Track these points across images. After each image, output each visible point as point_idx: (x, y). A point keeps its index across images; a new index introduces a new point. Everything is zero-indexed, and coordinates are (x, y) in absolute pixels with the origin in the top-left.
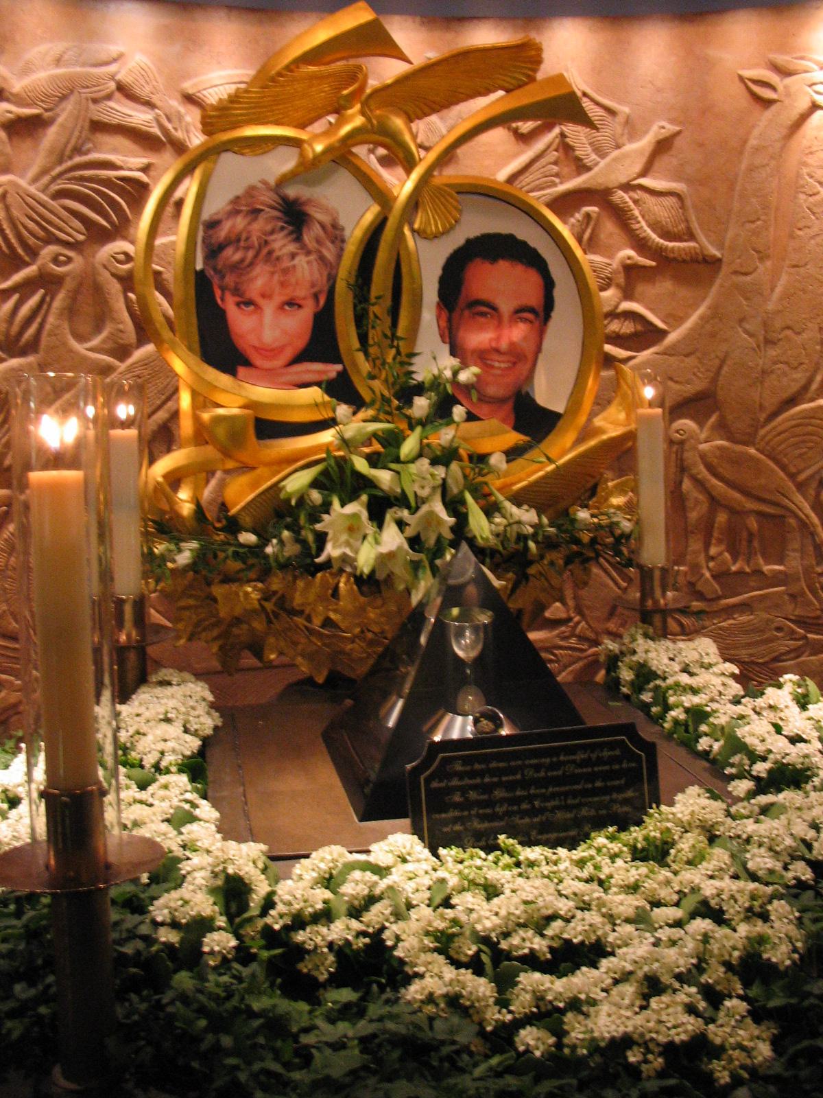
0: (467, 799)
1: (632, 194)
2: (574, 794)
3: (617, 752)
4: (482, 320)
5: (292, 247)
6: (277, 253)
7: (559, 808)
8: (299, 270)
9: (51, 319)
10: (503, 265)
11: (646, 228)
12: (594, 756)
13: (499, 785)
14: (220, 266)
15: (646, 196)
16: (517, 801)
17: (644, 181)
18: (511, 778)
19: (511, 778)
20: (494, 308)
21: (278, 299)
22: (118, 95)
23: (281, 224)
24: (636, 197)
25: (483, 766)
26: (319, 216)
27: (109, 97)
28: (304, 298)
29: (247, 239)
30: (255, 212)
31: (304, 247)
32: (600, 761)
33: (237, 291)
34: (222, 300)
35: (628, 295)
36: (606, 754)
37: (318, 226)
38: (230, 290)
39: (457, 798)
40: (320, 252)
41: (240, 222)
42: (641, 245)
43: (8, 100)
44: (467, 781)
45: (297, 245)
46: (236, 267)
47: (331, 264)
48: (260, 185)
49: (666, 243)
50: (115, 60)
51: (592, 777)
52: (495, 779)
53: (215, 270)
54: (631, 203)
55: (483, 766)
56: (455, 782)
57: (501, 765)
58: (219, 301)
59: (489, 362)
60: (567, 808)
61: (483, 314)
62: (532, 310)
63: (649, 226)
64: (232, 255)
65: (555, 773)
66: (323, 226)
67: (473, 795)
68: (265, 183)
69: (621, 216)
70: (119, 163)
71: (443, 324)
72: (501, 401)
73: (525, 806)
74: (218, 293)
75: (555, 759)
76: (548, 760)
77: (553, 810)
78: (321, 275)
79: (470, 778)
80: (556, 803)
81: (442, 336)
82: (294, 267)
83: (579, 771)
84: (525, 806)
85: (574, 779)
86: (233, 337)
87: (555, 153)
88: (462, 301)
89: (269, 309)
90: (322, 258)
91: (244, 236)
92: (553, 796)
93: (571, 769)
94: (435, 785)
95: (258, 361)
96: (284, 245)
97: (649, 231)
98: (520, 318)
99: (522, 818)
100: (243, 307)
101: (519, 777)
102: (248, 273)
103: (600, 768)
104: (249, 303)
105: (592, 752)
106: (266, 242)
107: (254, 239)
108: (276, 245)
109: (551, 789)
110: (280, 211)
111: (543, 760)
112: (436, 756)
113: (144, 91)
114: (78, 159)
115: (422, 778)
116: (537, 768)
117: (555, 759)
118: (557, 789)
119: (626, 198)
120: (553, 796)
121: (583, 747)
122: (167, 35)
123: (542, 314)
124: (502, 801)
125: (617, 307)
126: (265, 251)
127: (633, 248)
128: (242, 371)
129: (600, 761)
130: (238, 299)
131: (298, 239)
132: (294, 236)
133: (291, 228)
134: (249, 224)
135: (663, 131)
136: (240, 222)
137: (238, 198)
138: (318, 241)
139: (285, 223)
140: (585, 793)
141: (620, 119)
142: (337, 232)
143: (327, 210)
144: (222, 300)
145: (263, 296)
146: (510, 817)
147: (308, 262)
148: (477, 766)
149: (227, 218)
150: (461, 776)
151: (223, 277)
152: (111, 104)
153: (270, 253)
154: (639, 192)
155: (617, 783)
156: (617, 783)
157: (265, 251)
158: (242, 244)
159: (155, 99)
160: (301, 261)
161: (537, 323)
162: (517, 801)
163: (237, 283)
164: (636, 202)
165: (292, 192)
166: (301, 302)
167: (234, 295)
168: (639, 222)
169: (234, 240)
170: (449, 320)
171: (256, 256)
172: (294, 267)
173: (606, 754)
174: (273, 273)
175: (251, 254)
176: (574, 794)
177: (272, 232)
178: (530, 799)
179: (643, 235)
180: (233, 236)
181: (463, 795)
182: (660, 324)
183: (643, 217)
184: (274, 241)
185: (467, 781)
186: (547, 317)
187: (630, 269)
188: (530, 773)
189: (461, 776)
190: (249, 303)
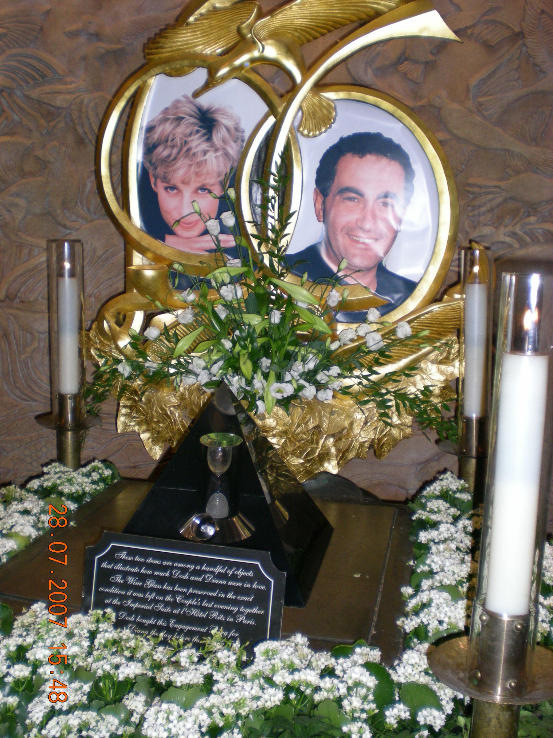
0: (126, 582)
2: (210, 599)
3: (250, 574)
4: (351, 204)
5: (204, 146)
7: (195, 607)
8: (209, 162)
10: (370, 158)
12: (230, 572)
13: (152, 576)
14: (154, 160)
16: (164, 593)
18: (161, 574)
19: (161, 574)
20: (362, 195)
21: (194, 185)
23: (196, 128)
25: (142, 560)
28: (213, 185)
29: (172, 140)
30: (179, 119)
31: (213, 145)
32: (234, 577)
33: (165, 179)
34: (155, 185)
36: (241, 573)
37: (224, 129)
38: (161, 179)
40: (224, 149)
41: (168, 127)
44: (128, 569)
45: (208, 144)
47: (233, 158)
48: (183, 99)
51: (226, 589)
52: (149, 572)
53: (150, 162)
55: (142, 560)
56: (119, 567)
57: (156, 562)
58: (153, 186)
59: (355, 238)
60: (203, 609)
61: (351, 199)
64: (162, 152)
65: (196, 579)
66: (228, 130)
67: (131, 580)
68: (186, 97)
71: (319, 206)
72: (369, 270)
73: (169, 598)
74: (152, 180)
75: (198, 568)
76: (192, 567)
77: (191, 606)
78: (225, 166)
79: (131, 567)
80: (194, 602)
81: (318, 216)
82: (206, 161)
83: (216, 581)
84: (169, 598)
85: (212, 587)
87: (516, 61)
88: (335, 187)
89: (187, 192)
90: (226, 154)
91: (170, 139)
92: (192, 596)
93: (210, 578)
94: (104, 565)
96: (199, 145)
98: (344, 199)
99: (164, 607)
100: (169, 190)
101: (167, 574)
102: (174, 165)
103: (234, 584)
104: (173, 188)
105: (230, 568)
106: (186, 142)
107: (178, 141)
109: (191, 591)
110: (196, 118)
111: (188, 566)
112: (110, 544)
115: (96, 557)
116: (184, 571)
117: (198, 568)
118: (196, 592)
120: (192, 596)
121: (224, 563)
124: (152, 590)
126: (185, 149)
129: (234, 577)
130: (166, 185)
131: (209, 139)
132: (206, 137)
133: (204, 131)
136: (168, 127)
137: (167, 109)
138: (224, 141)
139: (200, 127)
140: (217, 600)
142: (239, 134)
143: (230, 117)
145: (183, 182)
146: (156, 604)
147: (216, 157)
148: (137, 559)
149: (159, 125)
150: (125, 563)
151: (156, 168)
153: (189, 150)
155: (246, 599)
156: (246, 599)
157: (185, 149)
158: (169, 143)
160: (211, 156)
162: (164, 593)
163: (165, 173)
165: (205, 100)
166: (211, 188)
167: (163, 182)
169: (164, 141)
170: (324, 203)
171: (179, 153)
172: (206, 161)
173: (241, 573)
174: (191, 166)
175: (175, 151)
176: (210, 599)
177: (191, 134)
178: (174, 593)
180: (163, 138)
181: (123, 578)
184: (192, 140)
185: (128, 569)
188: (177, 574)
189: (125, 563)
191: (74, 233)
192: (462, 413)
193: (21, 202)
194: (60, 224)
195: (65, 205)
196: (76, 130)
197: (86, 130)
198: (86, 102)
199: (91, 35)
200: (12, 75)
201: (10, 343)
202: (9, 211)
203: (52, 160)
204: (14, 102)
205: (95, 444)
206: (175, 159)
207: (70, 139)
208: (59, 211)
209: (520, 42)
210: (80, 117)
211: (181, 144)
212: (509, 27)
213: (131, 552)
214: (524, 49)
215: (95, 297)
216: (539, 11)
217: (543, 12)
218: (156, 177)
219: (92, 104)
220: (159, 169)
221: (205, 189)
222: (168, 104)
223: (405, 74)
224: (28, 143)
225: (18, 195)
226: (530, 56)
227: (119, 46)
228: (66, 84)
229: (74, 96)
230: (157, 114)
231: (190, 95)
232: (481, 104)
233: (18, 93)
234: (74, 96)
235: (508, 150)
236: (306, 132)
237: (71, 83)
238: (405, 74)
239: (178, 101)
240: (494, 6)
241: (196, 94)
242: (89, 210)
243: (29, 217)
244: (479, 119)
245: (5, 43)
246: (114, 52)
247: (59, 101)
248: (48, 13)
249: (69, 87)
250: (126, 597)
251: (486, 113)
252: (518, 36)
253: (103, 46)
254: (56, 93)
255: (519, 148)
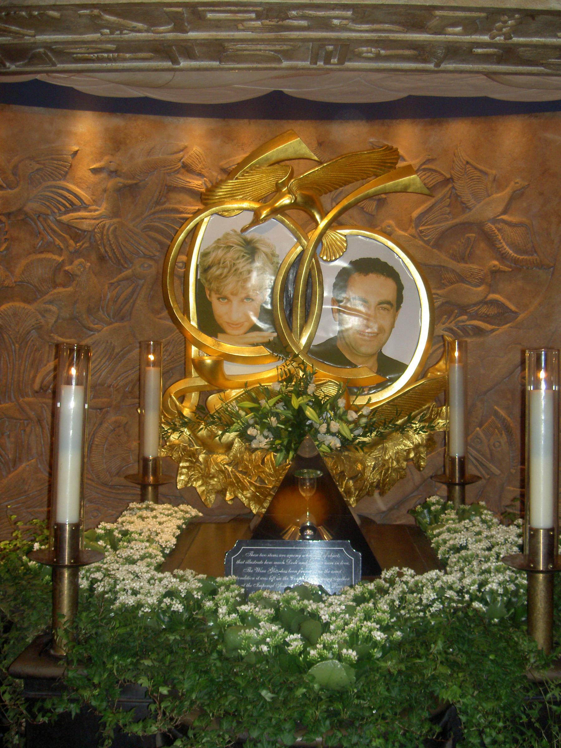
0: (254, 571)
1: (497, 225)
6: (241, 270)
9: (139, 301)
11: (505, 247)
14: (208, 278)
15: (506, 228)
17: (504, 217)
22: (182, 170)
24: (499, 226)
26: (263, 249)
27: (177, 172)
29: (224, 263)
30: (230, 247)
33: (218, 291)
34: (210, 296)
35: (492, 289)
39: (249, 570)
42: (503, 257)
43: (120, 176)
44: (255, 562)
46: (219, 278)
49: (518, 257)
50: (182, 150)
52: (270, 563)
53: (206, 279)
54: (496, 231)
56: (249, 562)
62: (389, 303)
63: (508, 245)
64: (216, 271)
66: (266, 255)
67: (258, 570)
69: (490, 240)
70: (181, 210)
74: (208, 293)
86: (217, 318)
87: (448, 200)
89: (235, 301)
91: (222, 262)
94: (238, 562)
95: (229, 330)
96: (245, 266)
97: (507, 248)
104: (225, 298)
107: (228, 262)
108: (240, 266)
113: (198, 167)
114: (158, 208)
119: (493, 227)
122: (212, 134)
123: (395, 306)
125: (486, 297)
126: (233, 269)
127: (497, 260)
128: (220, 335)
130: (218, 296)
133: (248, 256)
134: (225, 254)
135: (517, 185)
136: (220, 253)
137: (219, 240)
141: (491, 178)
143: (268, 246)
144: (210, 296)
145: (232, 294)
148: (261, 555)
150: (253, 559)
151: (211, 284)
152: (179, 176)
154: (501, 224)
157: (233, 269)
158: (221, 265)
159: (204, 171)
161: (392, 311)
163: (218, 287)
164: (499, 230)
165: (249, 235)
168: (501, 243)
171: (229, 272)
174: (238, 281)
175: (226, 270)
177: (238, 259)
179: (504, 251)
182: (513, 308)
183: (504, 240)
185: (255, 562)
186: (398, 307)
187: (495, 272)
190: (225, 298)
191: (96, 334)
192: (448, 455)
193: (54, 308)
194: (85, 327)
195: (89, 311)
196: (99, 249)
197: (107, 249)
198: (107, 226)
199: (112, 172)
200: (47, 203)
201: (43, 428)
202: (43, 316)
203: (79, 273)
204: (49, 226)
205: (114, 512)
206: (226, 277)
207: (94, 257)
208: (84, 316)
209: (450, 186)
210: (102, 239)
211: (231, 266)
212: (442, 174)
213: (256, 551)
214: (454, 190)
215: (113, 387)
216: (465, 163)
217: (467, 163)
218: (210, 290)
219: (111, 228)
220: (213, 284)
221: (249, 299)
222: (220, 236)
223: (363, 208)
224: (60, 259)
225: (51, 302)
226: (457, 196)
227: (135, 182)
228: (90, 211)
229: (97, 222)
230: (210, 243)
231: (239, 231)
232: (421, 232)
233: (51, 218)
234: (97, 222)
235: (443, 267)
236: (325, 258)
237: (95, 210)
238: (363, 208)
239: (228, 234)
240: (430, 157)
241: (244, 230)
242: (109, 315)
243: (60, 321)
244: (421, 243)
245: (42, 176)
246: (130, 186)
247: (86, 225)
248: (76, 153)
249: (93, 213)
250: (256, 582)
251: (426, 239)
252: (448, 181)
253: (120, 181)
254: (83, 218)
255: (452, 264)
